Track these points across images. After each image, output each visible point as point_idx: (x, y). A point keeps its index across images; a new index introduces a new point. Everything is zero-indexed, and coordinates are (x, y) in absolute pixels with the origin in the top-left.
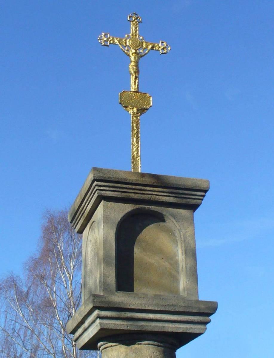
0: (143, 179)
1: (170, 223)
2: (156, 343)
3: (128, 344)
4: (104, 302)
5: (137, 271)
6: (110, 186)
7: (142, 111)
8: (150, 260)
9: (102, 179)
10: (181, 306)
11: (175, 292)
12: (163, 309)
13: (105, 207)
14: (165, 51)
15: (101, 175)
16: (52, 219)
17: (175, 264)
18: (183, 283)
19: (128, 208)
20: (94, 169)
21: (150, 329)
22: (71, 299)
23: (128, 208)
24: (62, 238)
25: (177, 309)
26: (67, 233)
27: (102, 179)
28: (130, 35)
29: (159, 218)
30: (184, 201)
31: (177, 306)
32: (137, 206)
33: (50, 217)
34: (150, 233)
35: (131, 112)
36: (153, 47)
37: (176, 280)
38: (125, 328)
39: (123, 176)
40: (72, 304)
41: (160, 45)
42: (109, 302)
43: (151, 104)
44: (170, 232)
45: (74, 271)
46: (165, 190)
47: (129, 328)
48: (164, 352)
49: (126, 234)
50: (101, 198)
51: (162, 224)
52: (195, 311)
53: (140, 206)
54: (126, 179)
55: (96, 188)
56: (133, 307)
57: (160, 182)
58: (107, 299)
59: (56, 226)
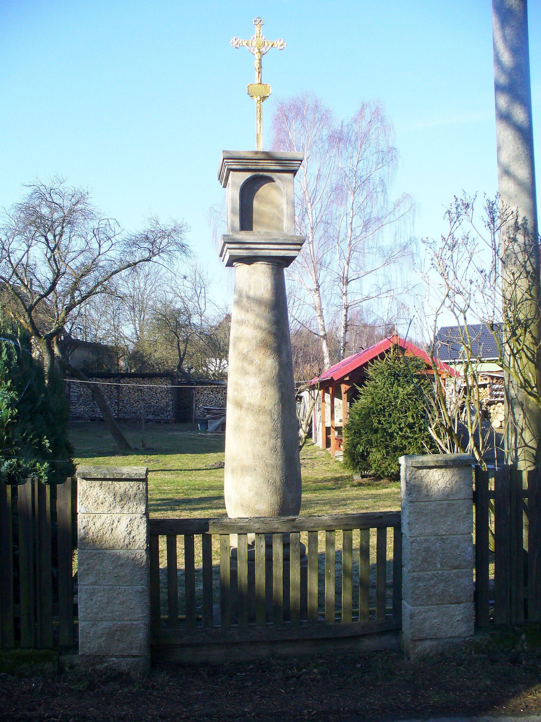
0: (257, 155)
1: (278, 182)
2: (267, 263)
3: (249, 264)
4: (230, 239)
5: (255, 217)
6: (233, 162)
7: (264, 98)
8: (263, 208)
9: (229, 157)
10: (280, 240)
11: (280, 229)
12: (269, 242)
13: (233, 176)
14: (282, 48)
15: (228, 155)
16: (281, 107)
17: (281, 212)
18: (286, 224)
19: (248, 175)
20: (224, 151)
21: (261, 255)
22: (306, 193)
23: (248, 175)
24: (294, 127)
25: (278, 242)
26: (299, 122)
27: (229, 157)
28: (255, 37)
29: (271, 180)
30: (286, 168)
31: (278, 239)
32: (254, 173)
33: (279, 104)
34: (264, 190)
35: (256, 99)
36: (273, 45)
37: (280, 220)
38: (245, 255)
39: (243, 155)
40: (307, 199)
41: (278, 41)
42: (234, 239)
43: (271, 93)
44: (278, 188)
45: (308, 163)
46: (272, 162)
47: (248, 254)
48: (273, 269)
49: (248, 192)
50: (230, 170)
51: (273, 183)
52: (290, 242)
53: (256, 173)
54: (245, 157)
55: (226, 164)
56: (249, 241)
57: (269, 157)
58: (232, 238)
59: (287, 114)
